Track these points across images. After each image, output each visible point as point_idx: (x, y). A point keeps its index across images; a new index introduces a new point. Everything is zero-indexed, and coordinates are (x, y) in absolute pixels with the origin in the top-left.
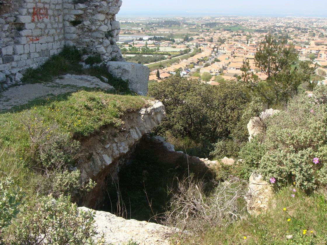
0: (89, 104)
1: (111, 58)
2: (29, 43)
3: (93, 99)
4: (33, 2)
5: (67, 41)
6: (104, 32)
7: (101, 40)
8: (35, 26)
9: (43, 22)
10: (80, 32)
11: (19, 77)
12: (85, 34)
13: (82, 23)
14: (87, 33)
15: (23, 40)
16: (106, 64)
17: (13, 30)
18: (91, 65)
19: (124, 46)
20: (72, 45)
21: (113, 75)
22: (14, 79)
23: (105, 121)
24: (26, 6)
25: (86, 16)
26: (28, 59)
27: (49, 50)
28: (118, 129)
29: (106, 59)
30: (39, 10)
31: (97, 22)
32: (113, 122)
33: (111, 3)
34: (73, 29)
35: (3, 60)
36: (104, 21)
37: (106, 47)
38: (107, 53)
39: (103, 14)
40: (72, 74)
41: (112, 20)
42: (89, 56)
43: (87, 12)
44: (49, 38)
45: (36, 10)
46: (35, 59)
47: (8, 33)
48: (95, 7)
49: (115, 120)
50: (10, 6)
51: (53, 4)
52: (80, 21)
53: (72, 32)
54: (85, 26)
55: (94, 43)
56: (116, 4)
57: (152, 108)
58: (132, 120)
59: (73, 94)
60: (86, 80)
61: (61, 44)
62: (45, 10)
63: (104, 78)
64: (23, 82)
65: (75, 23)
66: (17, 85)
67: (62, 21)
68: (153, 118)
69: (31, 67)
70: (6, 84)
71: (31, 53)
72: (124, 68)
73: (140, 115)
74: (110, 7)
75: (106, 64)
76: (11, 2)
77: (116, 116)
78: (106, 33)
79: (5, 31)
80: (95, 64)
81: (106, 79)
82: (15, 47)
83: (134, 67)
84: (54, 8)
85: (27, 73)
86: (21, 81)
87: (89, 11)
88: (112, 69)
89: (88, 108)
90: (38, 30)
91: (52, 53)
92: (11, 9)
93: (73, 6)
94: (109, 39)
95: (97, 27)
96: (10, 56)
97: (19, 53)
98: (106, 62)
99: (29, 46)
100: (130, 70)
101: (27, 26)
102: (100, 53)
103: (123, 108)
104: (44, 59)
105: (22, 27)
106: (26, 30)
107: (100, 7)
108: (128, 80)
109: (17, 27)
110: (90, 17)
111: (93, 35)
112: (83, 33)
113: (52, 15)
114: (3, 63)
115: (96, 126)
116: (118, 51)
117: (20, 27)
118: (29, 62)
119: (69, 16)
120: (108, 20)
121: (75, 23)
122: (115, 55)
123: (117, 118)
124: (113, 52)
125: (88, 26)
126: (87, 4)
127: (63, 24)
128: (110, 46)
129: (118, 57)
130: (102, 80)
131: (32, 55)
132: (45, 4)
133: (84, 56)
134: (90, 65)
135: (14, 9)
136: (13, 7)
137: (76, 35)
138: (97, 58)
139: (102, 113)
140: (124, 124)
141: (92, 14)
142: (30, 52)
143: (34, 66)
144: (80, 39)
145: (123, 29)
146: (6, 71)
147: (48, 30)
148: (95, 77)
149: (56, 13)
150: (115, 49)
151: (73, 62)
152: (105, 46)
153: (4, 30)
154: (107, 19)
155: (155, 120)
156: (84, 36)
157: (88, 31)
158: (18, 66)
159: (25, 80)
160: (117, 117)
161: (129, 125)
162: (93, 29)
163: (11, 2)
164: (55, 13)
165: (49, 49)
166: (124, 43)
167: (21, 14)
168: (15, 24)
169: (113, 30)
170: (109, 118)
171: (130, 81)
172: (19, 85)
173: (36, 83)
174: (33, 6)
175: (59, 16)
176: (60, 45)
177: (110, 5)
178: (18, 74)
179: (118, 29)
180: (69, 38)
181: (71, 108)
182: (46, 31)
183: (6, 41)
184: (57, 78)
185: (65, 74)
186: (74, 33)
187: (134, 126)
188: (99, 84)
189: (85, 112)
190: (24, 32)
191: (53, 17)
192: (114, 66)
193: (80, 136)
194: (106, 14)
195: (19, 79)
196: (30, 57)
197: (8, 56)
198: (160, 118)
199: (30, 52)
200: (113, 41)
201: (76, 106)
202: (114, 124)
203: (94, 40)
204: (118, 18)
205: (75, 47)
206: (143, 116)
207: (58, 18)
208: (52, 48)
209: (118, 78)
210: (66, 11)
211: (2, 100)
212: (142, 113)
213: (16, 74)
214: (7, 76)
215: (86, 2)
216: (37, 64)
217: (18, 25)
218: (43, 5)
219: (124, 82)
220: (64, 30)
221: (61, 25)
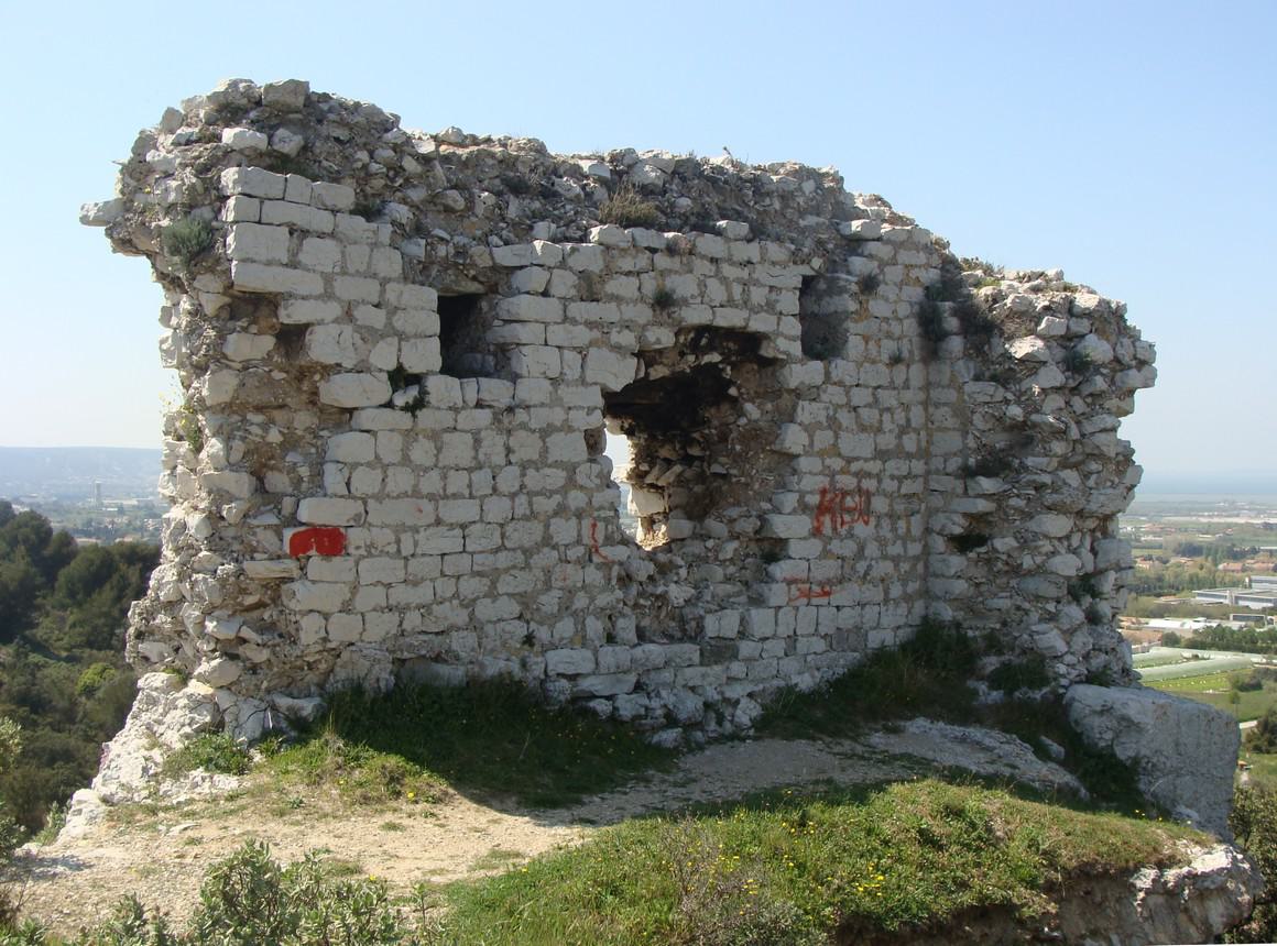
0: (938, 828)
1: (1086, 672)
2: (797, 603)
3: (955, 812)
4: (821, 473)
5: (934, 604)
6: (1065, 577)
7: (1051, 607)
8: (820, 549)
9: (851, 535)
10: (980, 573)
11: (747, 712)
12: (998, 581)
13: (989, 543)
14: (1005, 580)
15: (777, 594)
16: (1063, 695)
17: (750, 560)
18: (1010, 693)
19: (1271, 622)
20: (951, 619)
21: (1084, 737)
22: (729, 718)
23: (981, 893)
24: (798, 484)
25: (1004, 520)
26: (786, 655)
27: (867, 631)
28: (1028, 929)
29: (1063, 676)
30: (840, 496)
31: (1041, 543)
32: (1015, 900)
33: (1094, 477)
34: (957, 562)
35: (702, 654)
36: (1068, 537)
37: (1069, 634)
38: (1072, 653)
39: (1065, 514)
40: (934, 718)
41: (1099, 534)
42: (1003, 658)
43: (1007, 506)
44: (868, 589)
45: (828, 497)
46: (813, 656)
47: (731, 569)
48: (1036, 489)
49: (1020, 894)
50: (747, 485)
51: (892, 477)
52: (984, 536)
53: (953, 572)
54: (998, 552)
55: (1027, 614)
56: (1117, 480)
57: (1185, 870)
58: (1100, 904)
59: (896, 788)
60: (978, 743)
61: (909, 612)
62: (860, 496)
63: (1049, 742)
64: (757, 730)
65: (963, 543)
66: (736, 736)
67: (923, 533)
68: (1186, 910)
69: (794, 682)
70: (702, 730)
71: (800, 638)
72: (1124, 711)
73: (1132, 892)
74: (1091, 489)
75: (1063, 695)
76: (754, 471)
77: (1028, 883)
78: (1074, 581)
79: (725, 561)
80: (1024, 689)
81: (1056, 748)
82: (746, 613)
83: (1165, 713)
84: (895, 488)
85: (778, 701)
86: (753, 726)
87: (1013, 502)
88: (1083, 715)
89: (927, 839)
90: (832, 561)
91: (875, 639)
92: (751, 493)
93: (959, 485)
94: (1083, 603)
95: (1039, 560)
96: (728, 643)
97: (758, 635)
98: (1063, 686)
99: (794, 612)
100: (1147, 720)
101: (795, 548)
102: (1045, 652)
103: (1066, 857)
104: (844, 661)
105: (777, 550)
106: (787, 561)
107: (1055, 491)
108: (1136, 760)
109: (762, 550)
110: (1018, 523)
111: (1022, 586)
112: (991, 578)
113: (886, 515)
114: (702, 664)
115: (943, 906)
116: (1113, 649)
117: (774, 550)
118: (790, 665)
119: (947, 518)
120: (1083, 534)
121: (963, 543)
122: (1102, 665)
123: (1032, 889)
124: (1094, 649)
125: (1009, 556)
126: (1008, 479)
127: (923, 542)
128: (1085, 628)
129: (1116, 669)
130: (1042, 753)
131: (802, 645)
132: (863, 477)
133: (986, 660)
134: (1005, 694)
135: (759, 494)
136: (757, 486)
137: (966, 585)
138: (1035, 668)
139: (978, 865)
140: (1057, 914)
141: (1023, 512)
142: (795, 632)
143: (805, 682)
144: (981, 599)
145: (1271, 551)
146: (708, 688)
147: (867, 563)
148: (1014, 736)
149: (900, 507)
150: (1106, 642)
151: (945, 678)
152: (1065, 628)
153: (721, 557)
154: (1078, 531)
155: (1196, 920)
156: (994, 589)
157: (1007, 572)
158: (750, 677)
159: (766, 725)
160: (1031, 884)
161: (1081, 923)
162: (1025, 566)
163: (754, 471)
164: (896, 507)
165: (866, 627)
166: (1271, 609)
167: (777, 510)
168: (758, 540)
169: (1099, 573)
170: (1000, 884)
171: (1148, 762)
172: (743, 740)
173: (800, 737)
174: (821, 485)
175: (913, 518)
176: (907, 616)
177: (1091, 482)
178: (744, 702)
179: (1125, 569)
180: (939, 594)
181: (869, 832)
182: (861, 566)
183: (721, 593)
184: (879, 727)
185: (910, 719)
186: (959, 577)
187: (1105, 930)
188: (1018, 762)
189: (913, 851)
190: (781, 568)
191: (888, 521)
192: (1088, 702)
193: (871, 927)
194: (1077, 513)
195: (745, 720)
196: (795, 648)
197: (723, 643)
198: (1222, 916)
199: (795, 632)
200: (1097, 612)
201: (887, 829)
202: (1018, 908)
203: (1027, 605)
204: (1252, 506)
205: (958, 625)
206: (1141, 895)
207: (909, 523)
208: (878, 624)
209: (1103, 748)
210: (937, 501)
211: (671, 779)
212: (1139, 884)
213: (737, 702)
214: (707, 706)
215: (1007, 472)
216: (816, 673)
217: (766, 545)
218: (855, 480)
219: (1120, 763)
220: (926, 567)
221: (915, 549)
